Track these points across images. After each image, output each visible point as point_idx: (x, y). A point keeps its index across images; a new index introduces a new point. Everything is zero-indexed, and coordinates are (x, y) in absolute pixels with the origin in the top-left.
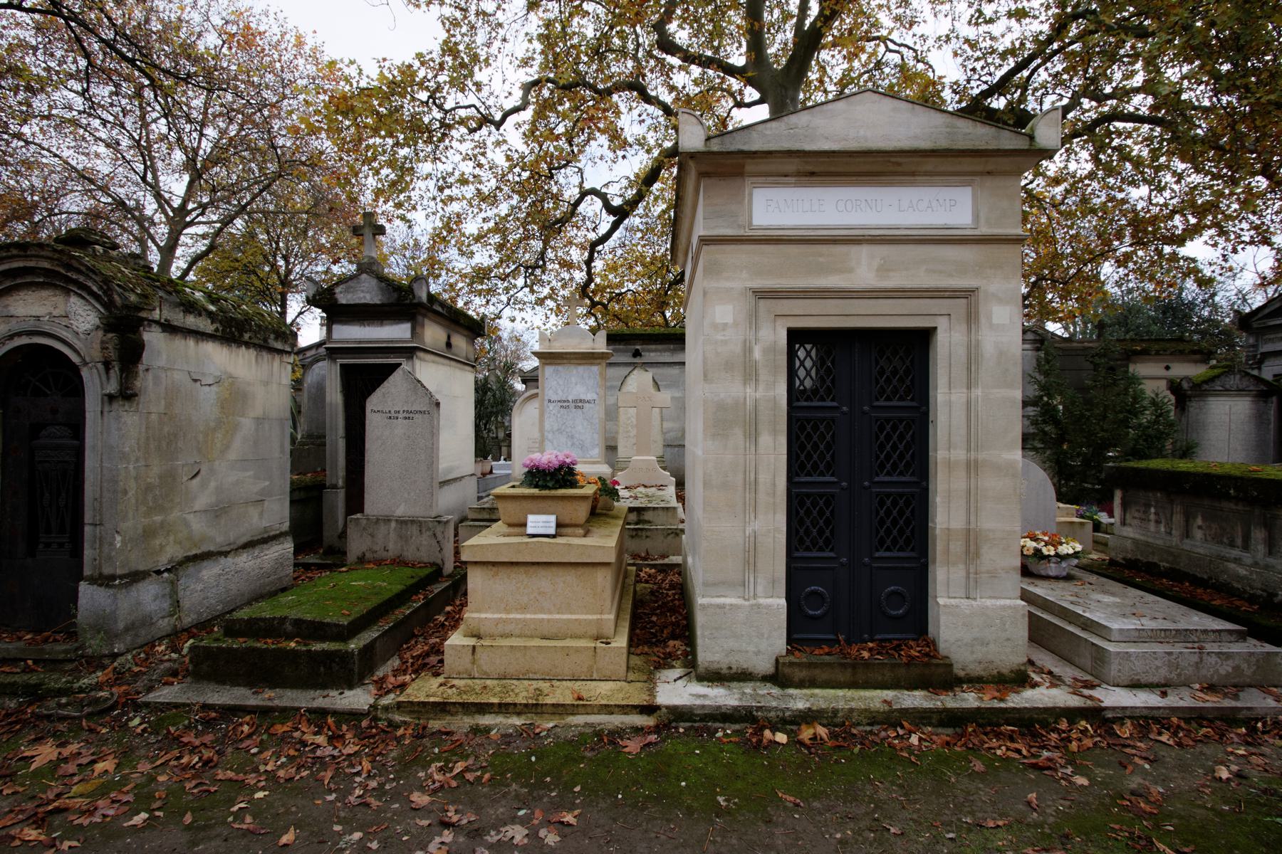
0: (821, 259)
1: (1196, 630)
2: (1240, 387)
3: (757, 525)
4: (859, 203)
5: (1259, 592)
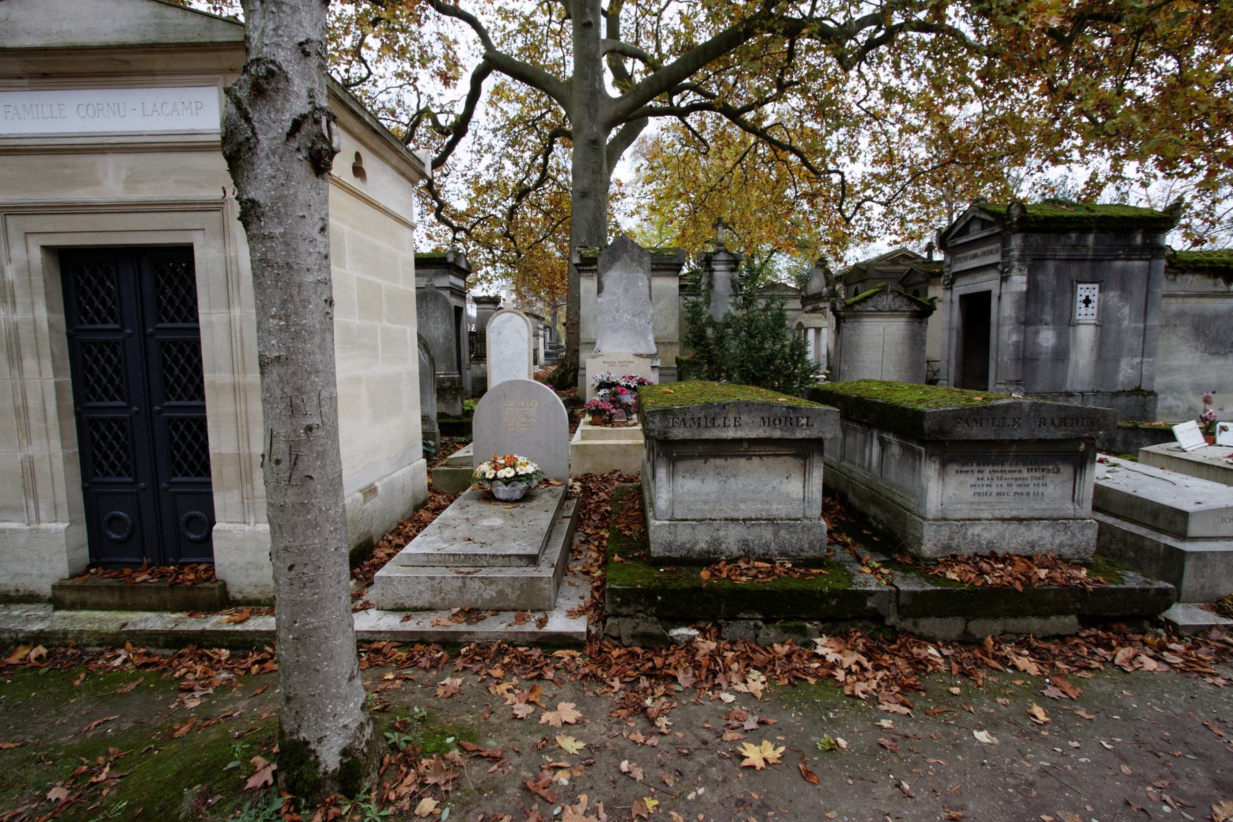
0: (67, 171)
1: (485, 555)
2: (893, 307)
3: (37, 449)
4: (100, 107)
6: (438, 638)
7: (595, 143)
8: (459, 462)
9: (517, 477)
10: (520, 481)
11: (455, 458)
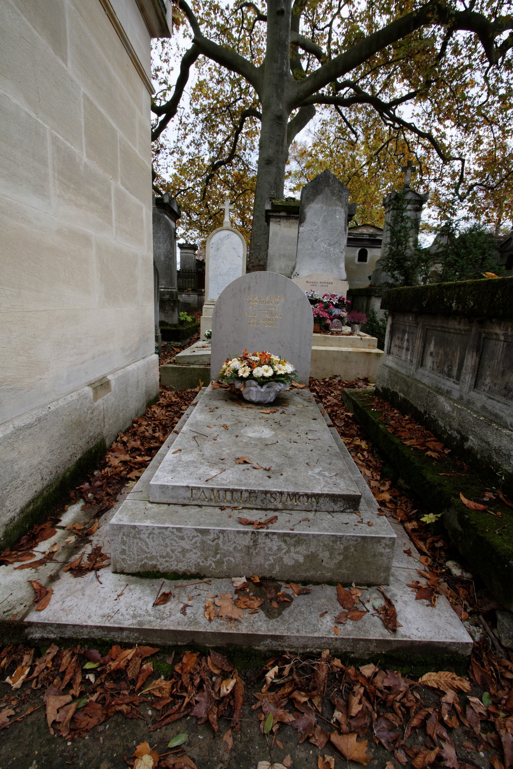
1: (281, 493)
5: (455, 434)
6: (219, 642)
7: (280, 119)
8: (187, 360)
9: (276, 378)
10: (277, 381)
11: (183, 357)
